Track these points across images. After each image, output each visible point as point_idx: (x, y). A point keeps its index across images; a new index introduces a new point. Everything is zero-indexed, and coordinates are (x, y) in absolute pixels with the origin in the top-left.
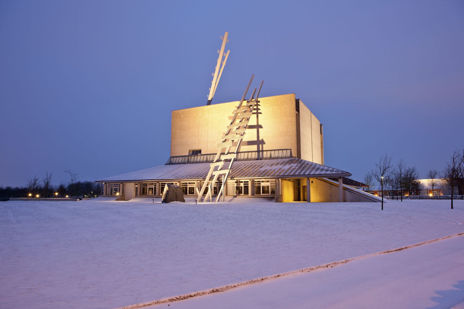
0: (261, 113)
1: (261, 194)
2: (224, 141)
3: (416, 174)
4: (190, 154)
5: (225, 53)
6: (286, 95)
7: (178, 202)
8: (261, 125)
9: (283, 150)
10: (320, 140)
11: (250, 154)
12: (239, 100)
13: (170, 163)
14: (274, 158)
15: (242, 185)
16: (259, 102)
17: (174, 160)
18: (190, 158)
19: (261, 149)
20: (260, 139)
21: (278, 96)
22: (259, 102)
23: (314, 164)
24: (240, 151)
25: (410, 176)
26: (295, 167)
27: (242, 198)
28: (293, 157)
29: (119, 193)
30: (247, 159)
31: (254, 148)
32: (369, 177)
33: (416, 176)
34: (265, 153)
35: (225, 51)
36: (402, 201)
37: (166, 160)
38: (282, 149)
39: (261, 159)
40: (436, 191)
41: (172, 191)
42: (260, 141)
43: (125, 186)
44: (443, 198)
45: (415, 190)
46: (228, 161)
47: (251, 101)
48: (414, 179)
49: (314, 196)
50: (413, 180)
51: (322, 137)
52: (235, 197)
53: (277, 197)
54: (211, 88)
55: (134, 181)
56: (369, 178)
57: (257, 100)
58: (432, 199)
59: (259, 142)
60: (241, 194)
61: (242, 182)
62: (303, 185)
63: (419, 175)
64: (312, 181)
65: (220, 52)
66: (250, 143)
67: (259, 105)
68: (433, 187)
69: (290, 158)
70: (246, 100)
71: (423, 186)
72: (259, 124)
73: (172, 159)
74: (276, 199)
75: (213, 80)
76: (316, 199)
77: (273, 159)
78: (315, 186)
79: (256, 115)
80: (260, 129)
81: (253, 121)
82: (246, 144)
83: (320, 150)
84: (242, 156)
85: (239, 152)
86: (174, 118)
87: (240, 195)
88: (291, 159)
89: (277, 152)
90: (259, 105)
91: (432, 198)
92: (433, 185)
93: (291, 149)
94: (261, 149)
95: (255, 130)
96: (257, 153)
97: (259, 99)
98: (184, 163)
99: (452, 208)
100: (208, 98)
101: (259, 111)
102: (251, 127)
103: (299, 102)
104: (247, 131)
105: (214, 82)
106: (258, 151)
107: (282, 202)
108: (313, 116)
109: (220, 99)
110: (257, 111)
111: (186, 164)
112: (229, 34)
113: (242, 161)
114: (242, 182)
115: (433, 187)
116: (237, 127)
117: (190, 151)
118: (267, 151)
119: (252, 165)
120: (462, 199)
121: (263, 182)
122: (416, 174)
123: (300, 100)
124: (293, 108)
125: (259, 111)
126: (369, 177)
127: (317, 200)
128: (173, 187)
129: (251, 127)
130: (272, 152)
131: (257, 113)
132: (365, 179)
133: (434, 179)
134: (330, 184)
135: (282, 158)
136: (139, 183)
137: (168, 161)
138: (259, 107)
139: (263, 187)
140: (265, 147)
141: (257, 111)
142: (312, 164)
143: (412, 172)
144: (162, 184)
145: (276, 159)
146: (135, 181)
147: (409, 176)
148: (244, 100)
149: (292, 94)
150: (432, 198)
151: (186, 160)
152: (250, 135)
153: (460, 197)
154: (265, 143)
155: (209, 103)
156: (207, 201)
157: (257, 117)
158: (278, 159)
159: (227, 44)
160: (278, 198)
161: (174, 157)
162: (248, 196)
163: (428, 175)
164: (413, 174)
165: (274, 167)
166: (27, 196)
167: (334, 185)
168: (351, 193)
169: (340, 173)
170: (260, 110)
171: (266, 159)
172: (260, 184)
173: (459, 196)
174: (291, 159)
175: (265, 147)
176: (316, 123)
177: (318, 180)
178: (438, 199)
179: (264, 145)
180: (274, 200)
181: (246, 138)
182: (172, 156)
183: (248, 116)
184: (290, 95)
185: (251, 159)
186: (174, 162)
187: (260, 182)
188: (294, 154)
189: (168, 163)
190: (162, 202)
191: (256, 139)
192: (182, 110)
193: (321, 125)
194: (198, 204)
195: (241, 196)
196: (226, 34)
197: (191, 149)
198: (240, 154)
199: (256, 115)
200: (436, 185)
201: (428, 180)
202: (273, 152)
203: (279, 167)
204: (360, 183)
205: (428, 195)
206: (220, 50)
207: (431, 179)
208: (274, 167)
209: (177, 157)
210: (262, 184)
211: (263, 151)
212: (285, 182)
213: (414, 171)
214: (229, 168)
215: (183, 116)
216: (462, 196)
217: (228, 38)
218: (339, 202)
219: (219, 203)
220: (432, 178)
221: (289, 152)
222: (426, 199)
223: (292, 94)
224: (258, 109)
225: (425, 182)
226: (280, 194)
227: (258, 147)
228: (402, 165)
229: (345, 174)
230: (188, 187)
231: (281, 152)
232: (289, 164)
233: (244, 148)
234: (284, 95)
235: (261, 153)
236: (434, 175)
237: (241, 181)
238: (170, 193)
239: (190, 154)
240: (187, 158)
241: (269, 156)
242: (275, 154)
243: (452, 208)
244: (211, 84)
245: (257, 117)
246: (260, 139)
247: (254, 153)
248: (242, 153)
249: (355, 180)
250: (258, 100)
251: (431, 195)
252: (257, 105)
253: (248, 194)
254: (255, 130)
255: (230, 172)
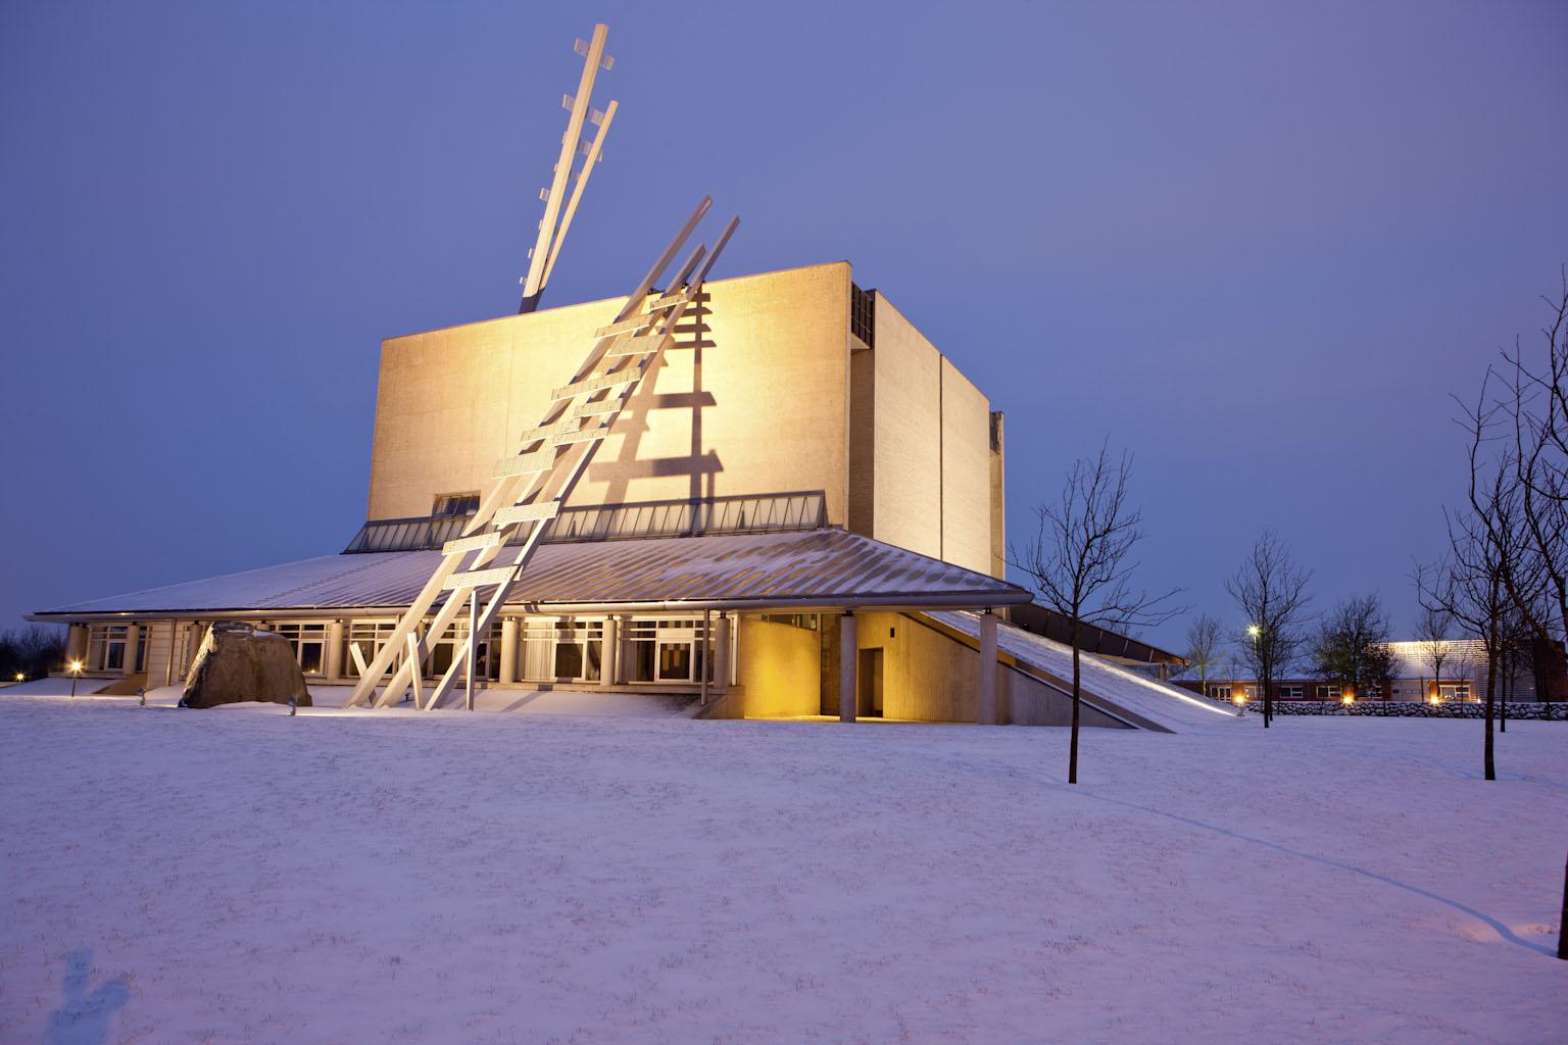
0: (711, 344)
1: (657, 680)
2: (526, 449)
3: (1378, 621)
4: (438, 512)
5: (597, 113)
6: (815, 269)
7: (271, 704)
8: (708, 395)
9: (790, 495)
10: (988, 473)
11: (661, 510)
12: (628, 295)
13: (365, 549)
14: (751, 531)
15: (582, 638)
16: (707, 297)
17: (379, 536)
18: (436, 525)
19: (704, 494)
20: (705, 451)
21: (782, 273)
22: (707, 297)
23: (895, 550)
24: (625, 501)
25: (1360, 627)
26: (812, 563)
27: (570, 698)
28: (831, 526)
29: (84, 664)
30: (650, 534)
31: (679, 486)
32: (1205, 629)
33: (1377, 629)
34: (719, 507)
35: (597, 103)
36: (1267, 726)
37: (349, 535)
38: (788, 490)
39: (700, 534)
40: (1455, 686)
41: (236, 655)
42: (705, 457)
43: (150, 637)
44: (1475, 711)
45: (1374, 681)
46: (575, 542)
47: (674, 292)
48: (1370, 637)
49: (897, 696)
50: (1366, 641)
51: (1000, 461)
52: (545, 688)
53: (707, 695)
54: (534, 247)
55: (172, 614)
56: (1207, 633)
57: (700, 289)
58: (1438, 715)
59: (699, 464)
60: (575, 680)
61: (581, 625)
62: (861, 648)
63: (1390, 623)
64: (893, 626)
65: (572, 104)
66: (666, 467)
67: (708, 312)
68: (1438, 668)
69: (815, 530)
70: (658, 292)
71: (1401, 663)
72: (704, 389)
73: (372, 530)
74: (706, 702)
75: (542, 217)
76: (905, 705)
77: (750, 533)
78: (903, 648)
79: (691, 352)
80: (706, 411)
81: (676, 374)
82: (651, 471)
83: (987, 513)
84: (629, 521)
85: (620, 506)
86: (389, 370)
87: (571, 683)
88: (822, 531)
89: (766, 504)
90: (708, 312)
91: (1437, 713)
92: (1439, 662)
93: (821, 494)
94: (704, 494)
95: (688, 412)
96: (691, 509)
97: (705, 289)
98: (412, 548)
99: (1490, 774)
100: (523, 287)
101: (705, 336)
102: (671, 401)
103: (872, 304)
104: (656, 417)
105: (546, 226)
106: (695, 502)
107: (741, 717)
108: (952, 374)
109: (562, 291)
110: (699, 336)
111: (417, 553)
112: (609, 31)
113: (626, 539)
114: (581, 625)
115: (1438, 668)
116: (593, 393)
117: (438, 501)
118: (727, 499)
119: (656, 554)
120: (1549, 718)
121: (664, 625)
122: (1378, 621)
123: (876, 293)
124: (838, 320)
125: (705, 336)
126: (1205, 629)
127: (907, 715)
128: (244, 635)
129: (671, 401)
130: (747, 503)
131: (699, 345)
132: (1192, 635)
133: (1443, 643)
134: (954, 642)
135: (783, 529)
136: (197, 623)
137: (357, 536)
138: (705, 319)
139: (663, 646)
140: (723, 485)
141: (699, 336)
142: (889, 552)
143: (1363, 615)
144: (284, 627)
145: (760, 533)
146: (176, 615)
147: (1353, 628)
148: (652, 291)
149: (835, 262)
150: (1437, 713)
151: (421, 538)
152: (668, 434)
153: (1541, 709)
154: (721, 469)
155: (530, 305)
156: (391, 706)
157: (698, 359)
158: (766, 532)
159: (601, 73)
160: (714, 701)
161: (378, 524)
162: (596, 688)
163: (1420, 621)
164: (1369, 620)
165: (730, 563)
166: (13, 679)
167: (968, 643)
168: (1029, 681)
169: (986, 588)
170: (709, 330)
171: (720, 533)
172: (653, 634)
173: (1535, 704)
174: (822, 531)
175: (723, 485)
176: (968, 407)
177: (911, 621)
178: (1456, 716)
179: (718, 476)
180: (693, 709)
181: (651, 448)
182: (372, 519)
183: (648, 349)
184: (831, 267)
185: (662, 535)
186: (377, 542)
187: (652, 624)
188: (838, 514)
189: (354, 547)
190: (180, 705)
191: (686, 451)
192: (420, 336)
193: (994, 418)
194: (300, 718)
195: (576, 688)
196: (600, 33)
197: (441, 491)
198: (623, 511)
199: (691, 352)
200: (1448, 663)
201: (1419, 643)
202: (750, 505)
203: (754, 560)
204: (1150, 648)
205: (1426, 700)
206: (574, 94)
207: (1433, 643)
208: (730, 563)
209: (388, 523)
210: (664, 636)
211: (711, 500)
212: (765, 634)
213: (1373, 610)
214: (518, 561)
215: (420, 361)
216: (1549, 706)
217: (608, 50)
218: (982, 723)
219: (438, 713)
220: (1437, 637)
221: (814, 502)
222: (1409, 715)
223: (840, 264)
224: (700, 328)
225: (1412, 653)
226: (734, 683)
227: (695, 485)
228: (1273, 556)
229: (1005, 592)
230: (301, 641)
231: (781, 503)
232: (796, 554)
233: (641, 489)
234: (805, 270)
235: (704, 507)
236: (1441, 626)
237: (579, 619)
238: (221, 662)
239: (438, 512)
240: (425, 526)
241: (733, 520)
242: (751, 511)
243: (1490, 774)
244: (537, 232)
245: (698, 359)
246: (705, 451)
247: (676, 510)
248: (631, 510)
249: (1156, 646)
250: (704, 291)
251: (1435, 700)
252: (700, 311)
253: (121, 667)
254: (686, 413)
255: (517, 578)
